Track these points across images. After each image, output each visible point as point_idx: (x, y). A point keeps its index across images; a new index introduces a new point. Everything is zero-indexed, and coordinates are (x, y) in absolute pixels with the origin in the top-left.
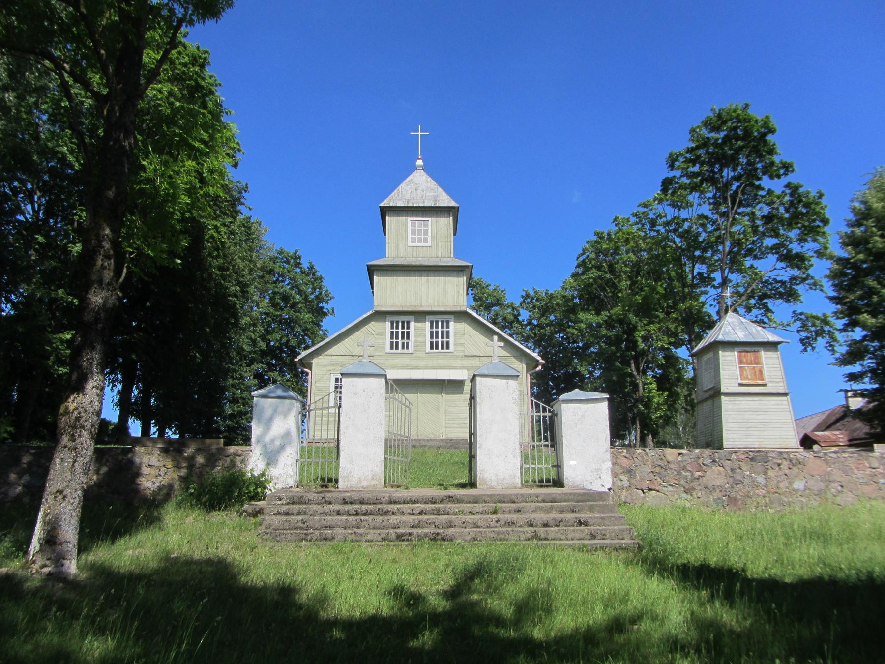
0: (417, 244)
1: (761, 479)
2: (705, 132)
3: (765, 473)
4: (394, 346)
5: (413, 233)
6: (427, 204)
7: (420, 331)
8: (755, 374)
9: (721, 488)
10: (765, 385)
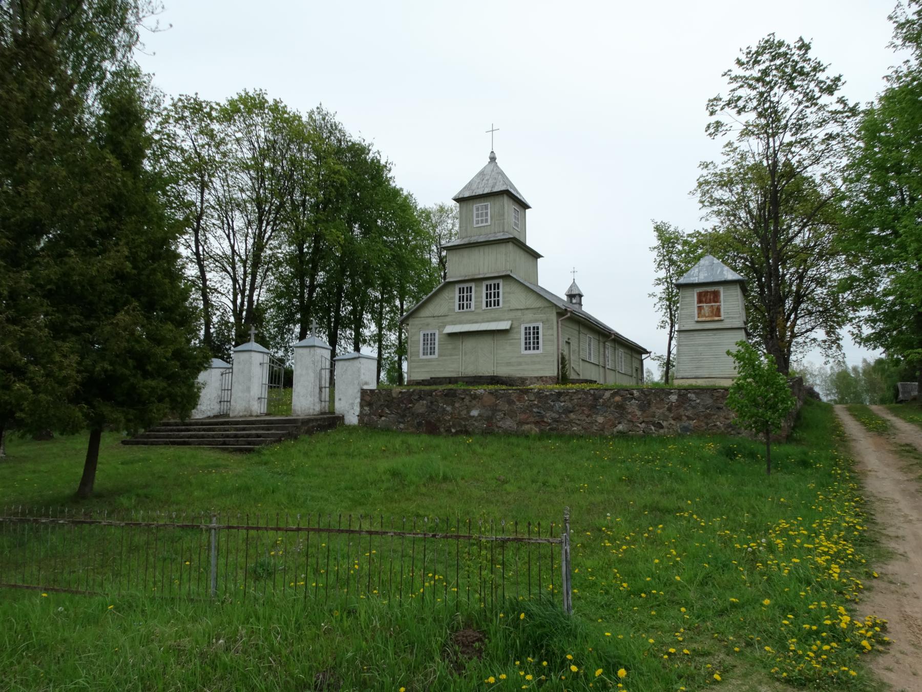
0: (480, 225)
1: (449, 409)
2: (738, 71)
3: (453, 405)
4: (461, 307)
5: (477, 216)
6: (485, 192)
7: (479, 294)
8: (712, 312)
9: (422, 415)
10: (721, 321)
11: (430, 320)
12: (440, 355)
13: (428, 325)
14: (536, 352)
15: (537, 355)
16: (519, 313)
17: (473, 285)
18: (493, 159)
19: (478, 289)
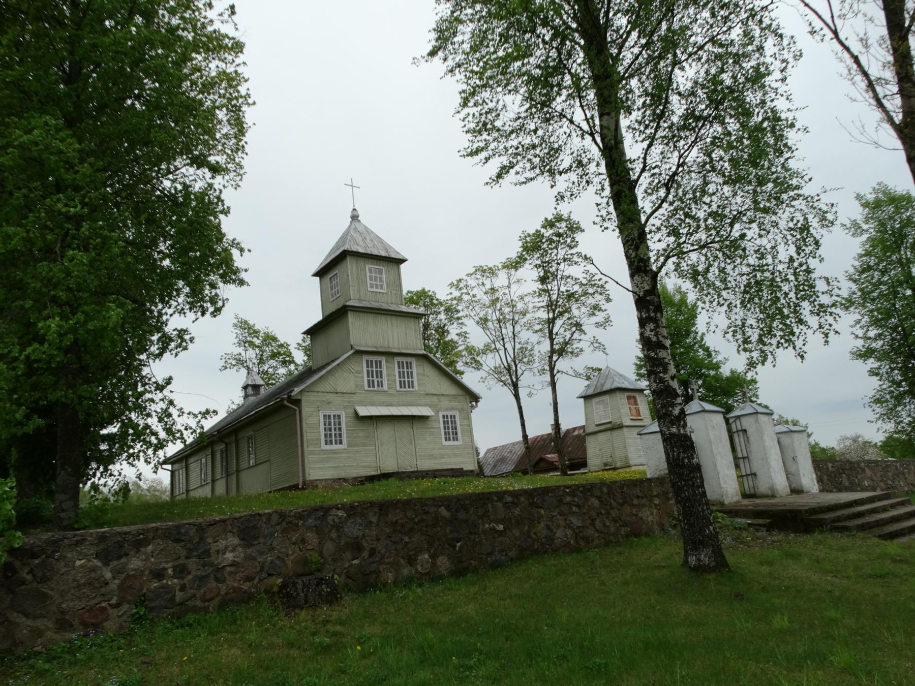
5: (371, 279)
11: (331, 397)
12: (349, 445)
13: (329, 403)
14: (455, 443)
15: (457, 447)
16: (435, 399)
17: (383, 359)
18: (355, 217)
19: (389, 365)
